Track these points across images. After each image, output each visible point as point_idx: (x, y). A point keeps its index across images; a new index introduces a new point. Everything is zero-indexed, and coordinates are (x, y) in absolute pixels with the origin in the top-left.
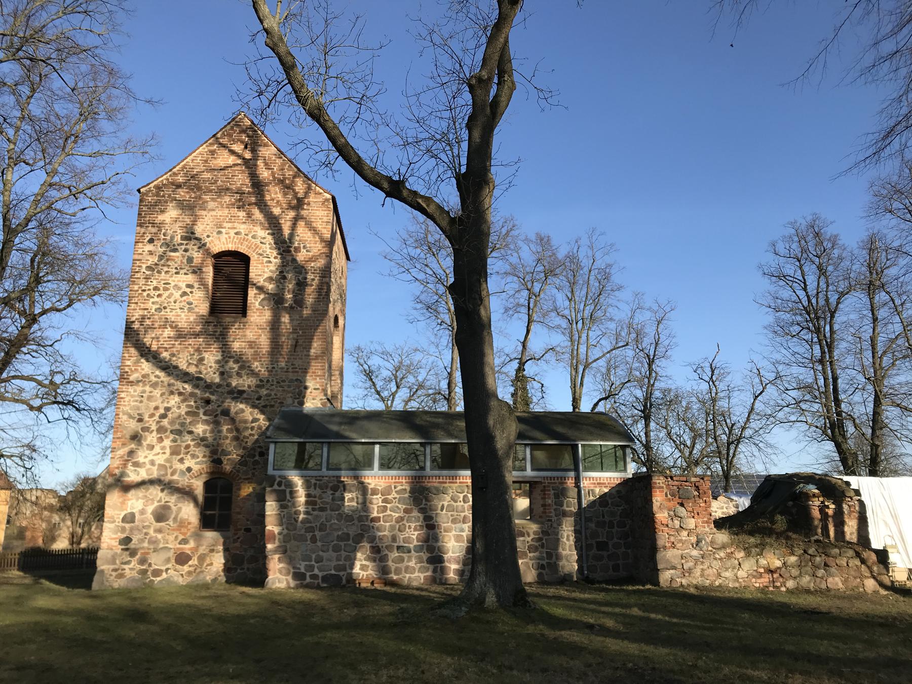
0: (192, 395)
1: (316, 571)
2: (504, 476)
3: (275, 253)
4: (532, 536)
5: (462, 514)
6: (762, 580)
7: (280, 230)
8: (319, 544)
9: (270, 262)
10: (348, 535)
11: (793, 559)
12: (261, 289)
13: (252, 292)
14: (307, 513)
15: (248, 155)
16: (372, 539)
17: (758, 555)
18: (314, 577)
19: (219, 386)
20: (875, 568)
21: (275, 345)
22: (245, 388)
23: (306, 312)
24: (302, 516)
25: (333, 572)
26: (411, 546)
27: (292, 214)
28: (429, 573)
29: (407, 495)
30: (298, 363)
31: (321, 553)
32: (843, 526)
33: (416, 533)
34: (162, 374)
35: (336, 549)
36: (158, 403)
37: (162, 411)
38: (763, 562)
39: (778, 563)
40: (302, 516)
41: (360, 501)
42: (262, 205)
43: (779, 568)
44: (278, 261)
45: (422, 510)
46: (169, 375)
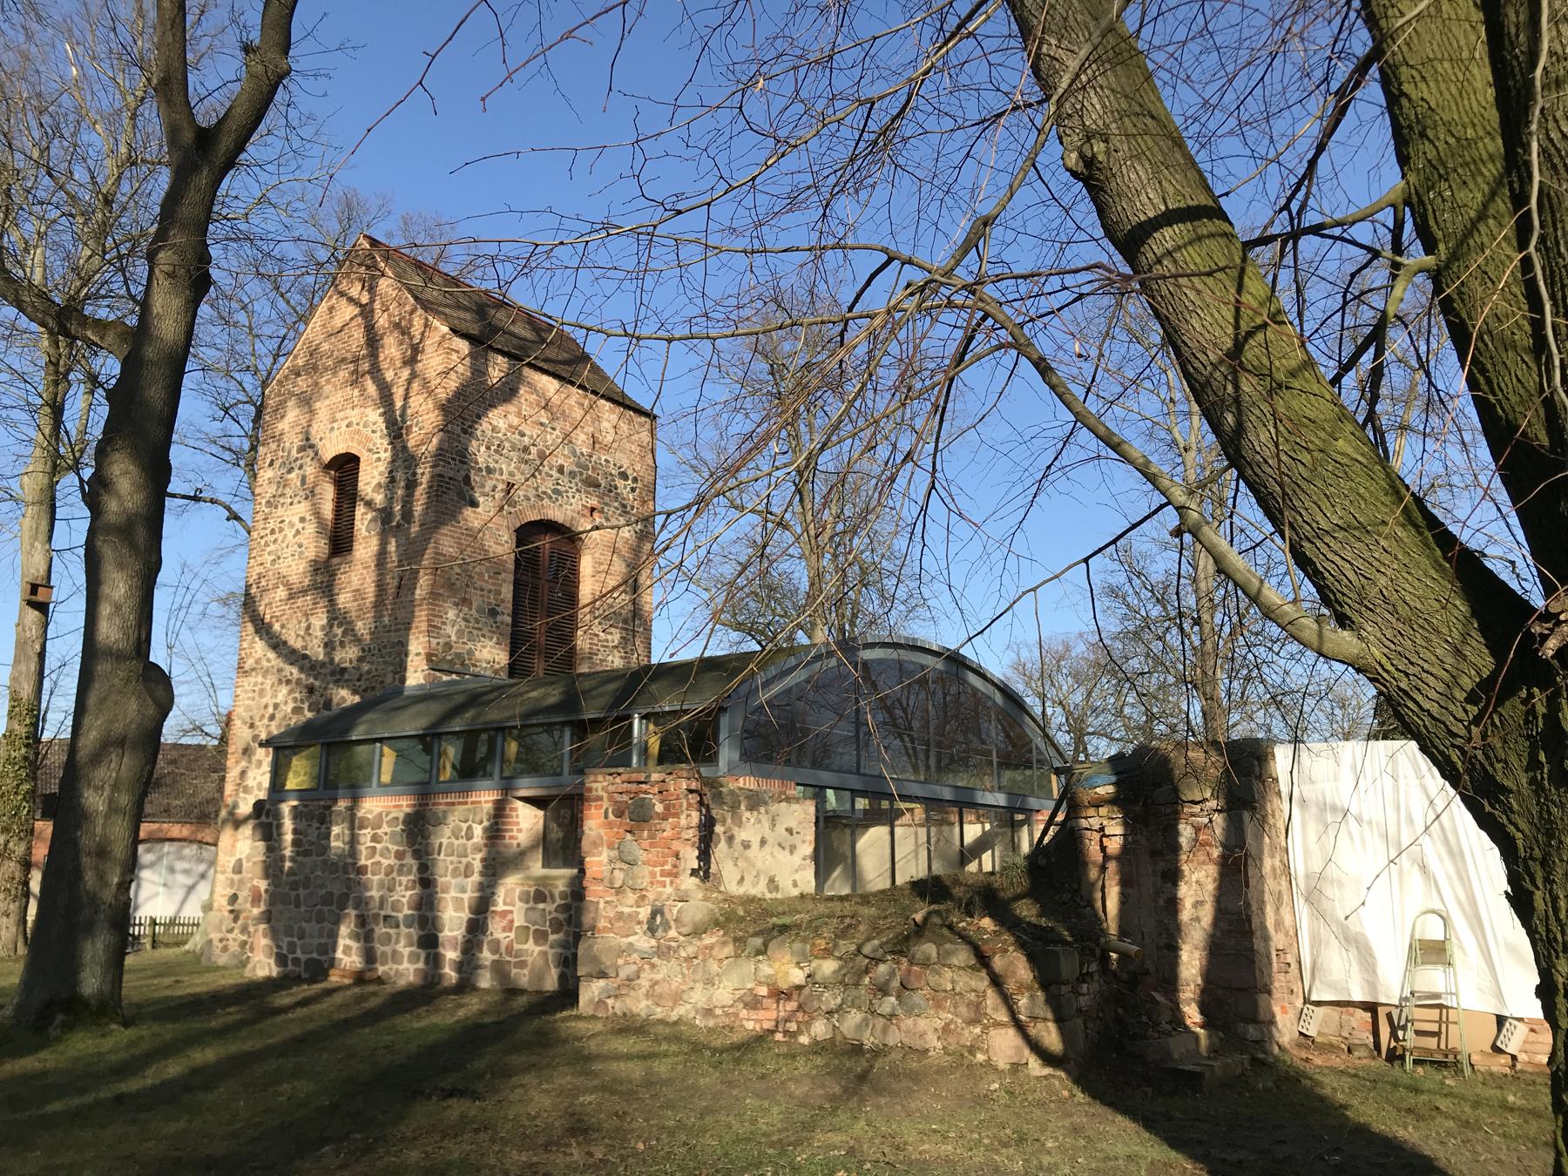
0: (298, 682)
1: (299, 954)
2: (81, 795)
3: (385, 442)
4: (559, 902)
5: (464, 860)
6: (761, 1014)
7: (392, 404)
8: (303, 909)
9: (379, 459)
10: (332, 894)
11: (828, 967)
12: (369, 504)
13: (360, 510)
14: (292, 859)
15: (365, 299)
16: (361, 903)
17: (758, 953)
18: (296, 961)
19: (323, 664)
20: (1023, 1002)
21: (381, 587)
22: (347, 665)
23: (415, 529)
24: (288, 864)
25: (315, 955)
26: (400, 916)
27: (406, 373)
28: (421, 965)
29: (398, 829)
30: (400, 614)
31: (304, 924)
32: (1175, 885)
33: (409, 893)
34: (271, 655)
35: (320, 920)
36: (267, 699)
37: (271, 710)
38: (766, 969)
39: (797, 976)
40: (288, 864)
41: (347, 839)
42: (375, 372)
43: (799, 988)
44: (388, 454)
45: (417, 854)
46: (279, 655)
